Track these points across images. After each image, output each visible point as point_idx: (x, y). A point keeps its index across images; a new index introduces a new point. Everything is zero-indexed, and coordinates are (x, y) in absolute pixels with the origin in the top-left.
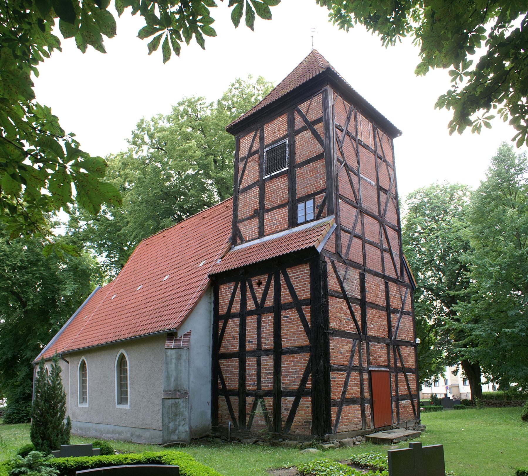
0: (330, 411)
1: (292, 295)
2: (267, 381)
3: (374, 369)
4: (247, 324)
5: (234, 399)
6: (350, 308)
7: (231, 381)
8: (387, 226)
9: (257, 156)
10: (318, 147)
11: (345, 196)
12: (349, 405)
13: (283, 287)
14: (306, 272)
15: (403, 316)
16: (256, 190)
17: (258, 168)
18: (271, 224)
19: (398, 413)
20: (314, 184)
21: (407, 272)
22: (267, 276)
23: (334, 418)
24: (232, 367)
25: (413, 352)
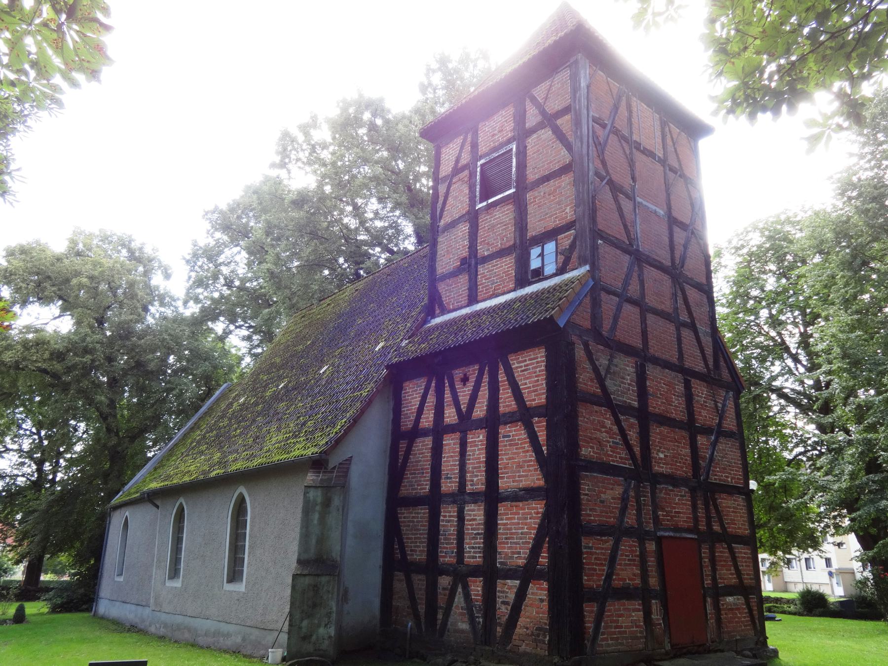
0: (581, 611)
2: (473, 548)
3: (667, 534)
4: (444, 447)
5: (418, 580)
6: (618, 422)
8: (687, 283)
9: (466, 173)
10: (562, 154)
12: (619, 599)
13: (502, 386)
14: (539, 359)
15: (722, 440)
16: (464, 229)
17: (467, 192)
18: (488, 282)
19: (719, 621)
20: (556, 214)
21: (726, 362)
22: (477, 367)
23: (590, 625)
24: (418, 522)
25: (744, 506)
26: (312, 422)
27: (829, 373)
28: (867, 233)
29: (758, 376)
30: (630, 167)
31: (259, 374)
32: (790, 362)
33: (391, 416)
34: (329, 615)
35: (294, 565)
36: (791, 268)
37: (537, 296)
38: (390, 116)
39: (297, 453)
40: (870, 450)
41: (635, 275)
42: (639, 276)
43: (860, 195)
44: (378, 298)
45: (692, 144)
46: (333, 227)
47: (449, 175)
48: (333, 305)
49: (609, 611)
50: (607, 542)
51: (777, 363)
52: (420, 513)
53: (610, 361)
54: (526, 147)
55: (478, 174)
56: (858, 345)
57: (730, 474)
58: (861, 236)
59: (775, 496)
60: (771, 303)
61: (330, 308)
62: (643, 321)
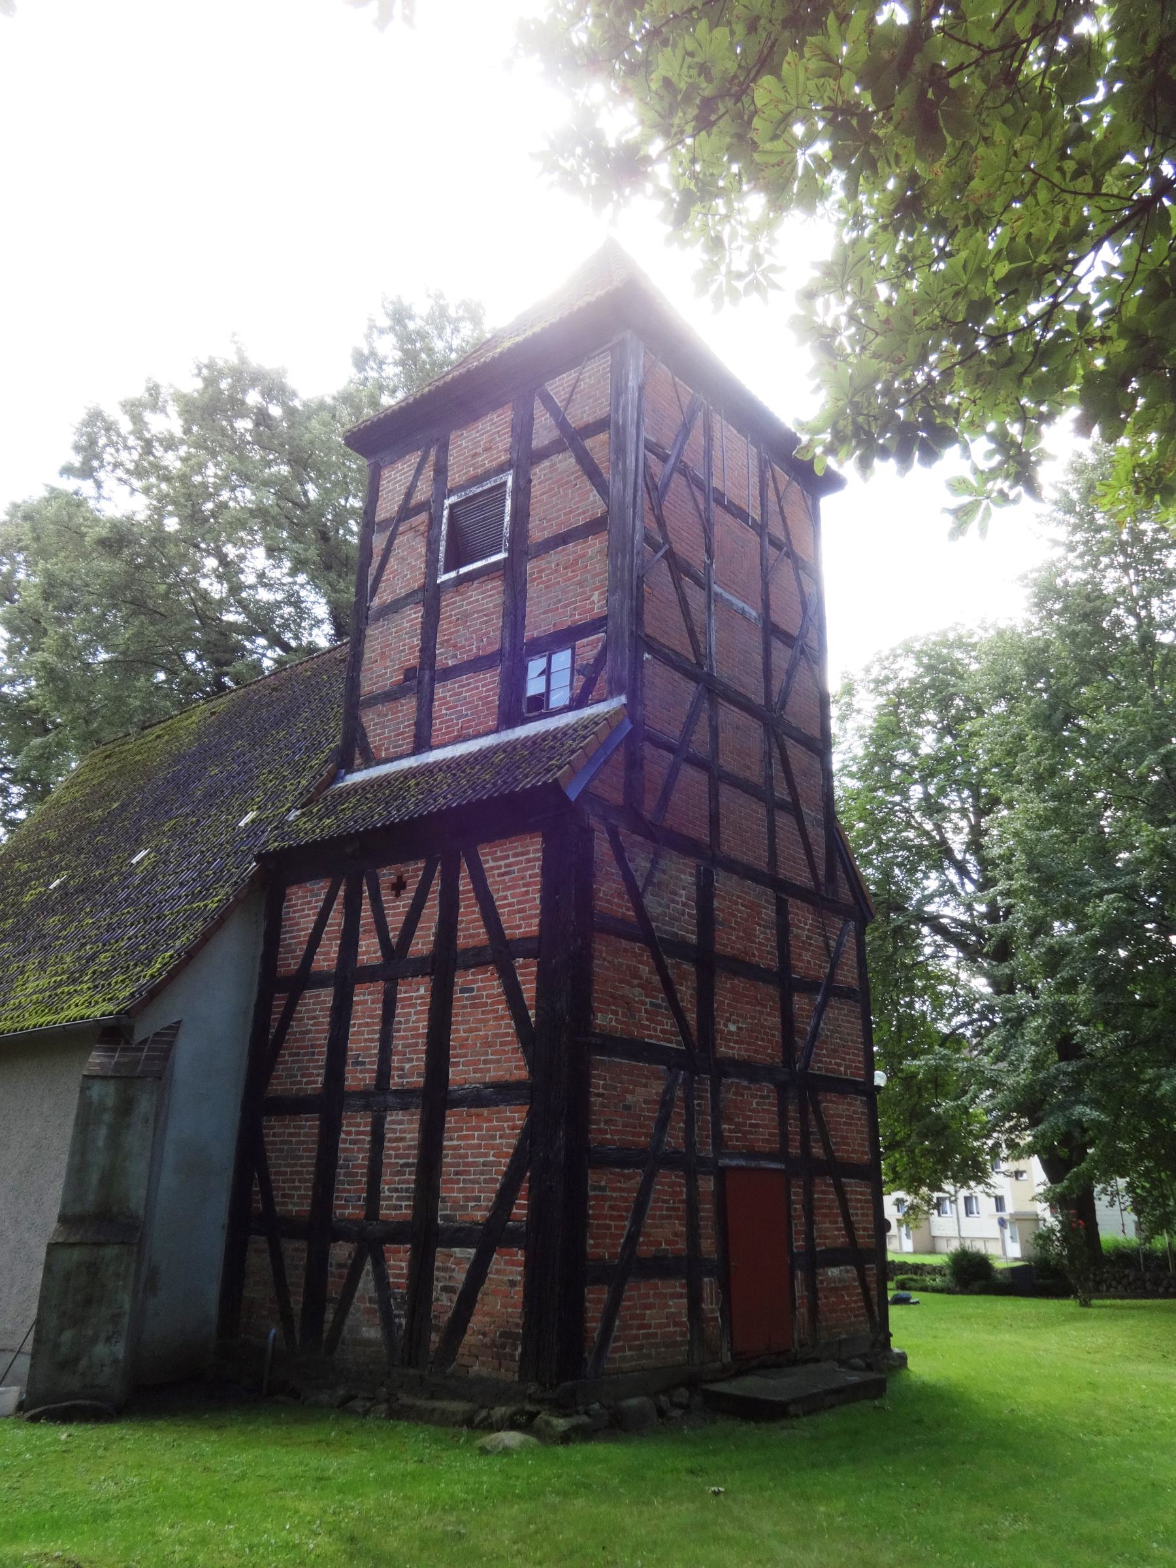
0: (582, 1299)
1: (487, 925)
2: (396, 1190)
3: (734, 1163)
4: (355, 1008)
6: (661, 968)
7: (289, 1189)
9: (423, 517)
10: (591, 499)
11: (662, 640)
13: (464, 900)
14: (531, 856)
15: (833, 1002)
16: (414, 615)
17: (424, 551)
18: (451, 714)
19: (814, 1310)
20: (575, 602)
21: (846, 871)
22: (421, 864)
23: (594, 1326)
24: (298, 1143)
25: (863, 1113)
26: (108, 954)
27: (1008, 894)
28: (1073, 669)
29: (901, 896)
30: (705, 530)
31: (13, 860)
32: (952, 875)
33: (261, 948)
34: (115, 1319)
35: (53, 1225)
36: (960, 719)
37: (534, 743)
38: (297, 403)
39: (73, 1012)
40: (1063, 1022)
41: (704, 717)
42: (710, 719)
43: (1065, 609)
44: (252, 730)
45: (810, 503)
46: (178, 594)
47: (392, 519)
48: (166, 737)
49: (630, 1299)
50: (629, 1178)
51: (933, 874)
52: (304, 1127)
53: (654, 863)
54: (530, 481)
55: (445, 520)
56: (1055, 851)
57: (844, 1059)
58: (1066, 674)
59: (920, 1096)
60: (928, 776)
61: (160, 744)
62: (714, 796)
